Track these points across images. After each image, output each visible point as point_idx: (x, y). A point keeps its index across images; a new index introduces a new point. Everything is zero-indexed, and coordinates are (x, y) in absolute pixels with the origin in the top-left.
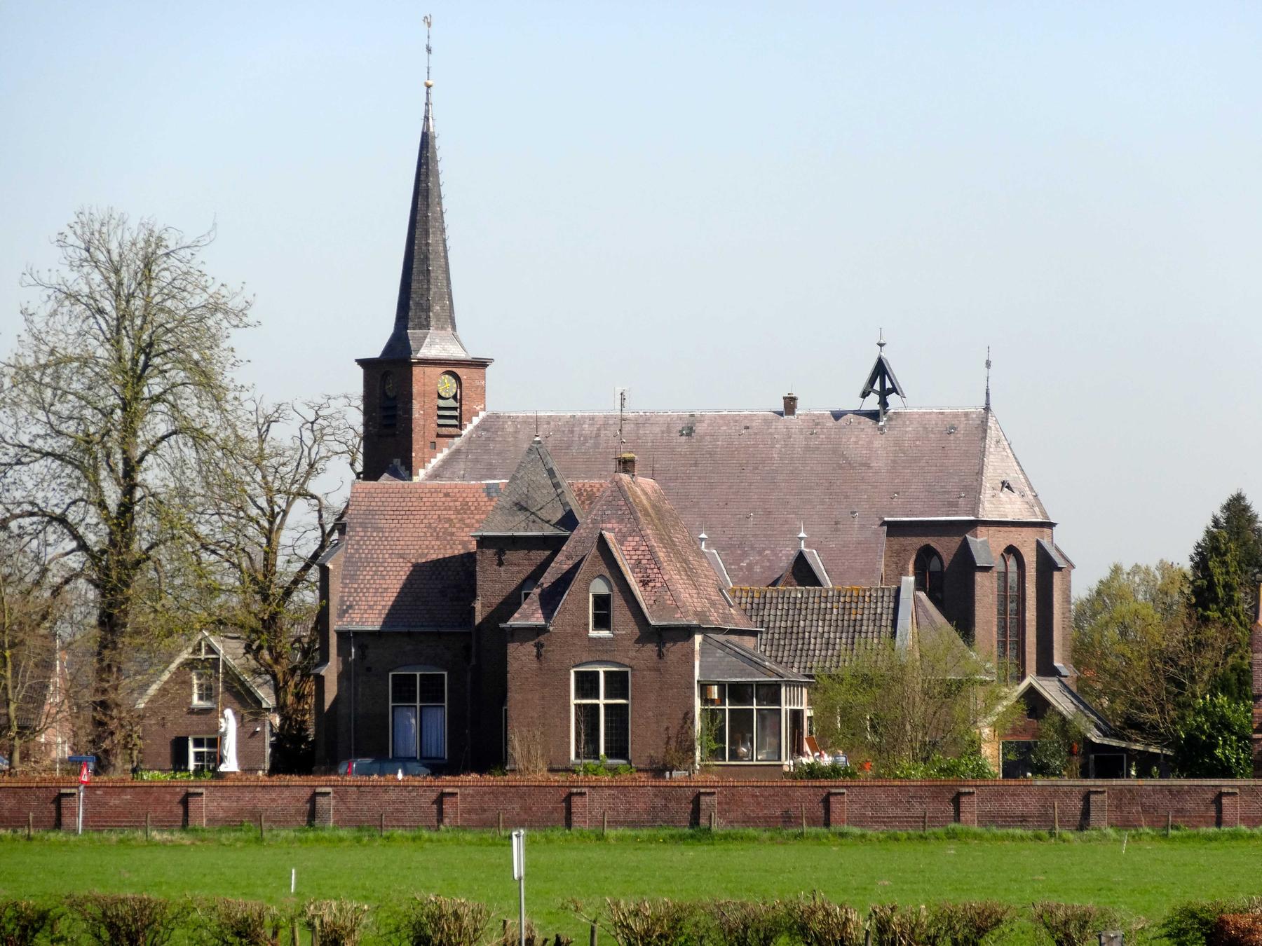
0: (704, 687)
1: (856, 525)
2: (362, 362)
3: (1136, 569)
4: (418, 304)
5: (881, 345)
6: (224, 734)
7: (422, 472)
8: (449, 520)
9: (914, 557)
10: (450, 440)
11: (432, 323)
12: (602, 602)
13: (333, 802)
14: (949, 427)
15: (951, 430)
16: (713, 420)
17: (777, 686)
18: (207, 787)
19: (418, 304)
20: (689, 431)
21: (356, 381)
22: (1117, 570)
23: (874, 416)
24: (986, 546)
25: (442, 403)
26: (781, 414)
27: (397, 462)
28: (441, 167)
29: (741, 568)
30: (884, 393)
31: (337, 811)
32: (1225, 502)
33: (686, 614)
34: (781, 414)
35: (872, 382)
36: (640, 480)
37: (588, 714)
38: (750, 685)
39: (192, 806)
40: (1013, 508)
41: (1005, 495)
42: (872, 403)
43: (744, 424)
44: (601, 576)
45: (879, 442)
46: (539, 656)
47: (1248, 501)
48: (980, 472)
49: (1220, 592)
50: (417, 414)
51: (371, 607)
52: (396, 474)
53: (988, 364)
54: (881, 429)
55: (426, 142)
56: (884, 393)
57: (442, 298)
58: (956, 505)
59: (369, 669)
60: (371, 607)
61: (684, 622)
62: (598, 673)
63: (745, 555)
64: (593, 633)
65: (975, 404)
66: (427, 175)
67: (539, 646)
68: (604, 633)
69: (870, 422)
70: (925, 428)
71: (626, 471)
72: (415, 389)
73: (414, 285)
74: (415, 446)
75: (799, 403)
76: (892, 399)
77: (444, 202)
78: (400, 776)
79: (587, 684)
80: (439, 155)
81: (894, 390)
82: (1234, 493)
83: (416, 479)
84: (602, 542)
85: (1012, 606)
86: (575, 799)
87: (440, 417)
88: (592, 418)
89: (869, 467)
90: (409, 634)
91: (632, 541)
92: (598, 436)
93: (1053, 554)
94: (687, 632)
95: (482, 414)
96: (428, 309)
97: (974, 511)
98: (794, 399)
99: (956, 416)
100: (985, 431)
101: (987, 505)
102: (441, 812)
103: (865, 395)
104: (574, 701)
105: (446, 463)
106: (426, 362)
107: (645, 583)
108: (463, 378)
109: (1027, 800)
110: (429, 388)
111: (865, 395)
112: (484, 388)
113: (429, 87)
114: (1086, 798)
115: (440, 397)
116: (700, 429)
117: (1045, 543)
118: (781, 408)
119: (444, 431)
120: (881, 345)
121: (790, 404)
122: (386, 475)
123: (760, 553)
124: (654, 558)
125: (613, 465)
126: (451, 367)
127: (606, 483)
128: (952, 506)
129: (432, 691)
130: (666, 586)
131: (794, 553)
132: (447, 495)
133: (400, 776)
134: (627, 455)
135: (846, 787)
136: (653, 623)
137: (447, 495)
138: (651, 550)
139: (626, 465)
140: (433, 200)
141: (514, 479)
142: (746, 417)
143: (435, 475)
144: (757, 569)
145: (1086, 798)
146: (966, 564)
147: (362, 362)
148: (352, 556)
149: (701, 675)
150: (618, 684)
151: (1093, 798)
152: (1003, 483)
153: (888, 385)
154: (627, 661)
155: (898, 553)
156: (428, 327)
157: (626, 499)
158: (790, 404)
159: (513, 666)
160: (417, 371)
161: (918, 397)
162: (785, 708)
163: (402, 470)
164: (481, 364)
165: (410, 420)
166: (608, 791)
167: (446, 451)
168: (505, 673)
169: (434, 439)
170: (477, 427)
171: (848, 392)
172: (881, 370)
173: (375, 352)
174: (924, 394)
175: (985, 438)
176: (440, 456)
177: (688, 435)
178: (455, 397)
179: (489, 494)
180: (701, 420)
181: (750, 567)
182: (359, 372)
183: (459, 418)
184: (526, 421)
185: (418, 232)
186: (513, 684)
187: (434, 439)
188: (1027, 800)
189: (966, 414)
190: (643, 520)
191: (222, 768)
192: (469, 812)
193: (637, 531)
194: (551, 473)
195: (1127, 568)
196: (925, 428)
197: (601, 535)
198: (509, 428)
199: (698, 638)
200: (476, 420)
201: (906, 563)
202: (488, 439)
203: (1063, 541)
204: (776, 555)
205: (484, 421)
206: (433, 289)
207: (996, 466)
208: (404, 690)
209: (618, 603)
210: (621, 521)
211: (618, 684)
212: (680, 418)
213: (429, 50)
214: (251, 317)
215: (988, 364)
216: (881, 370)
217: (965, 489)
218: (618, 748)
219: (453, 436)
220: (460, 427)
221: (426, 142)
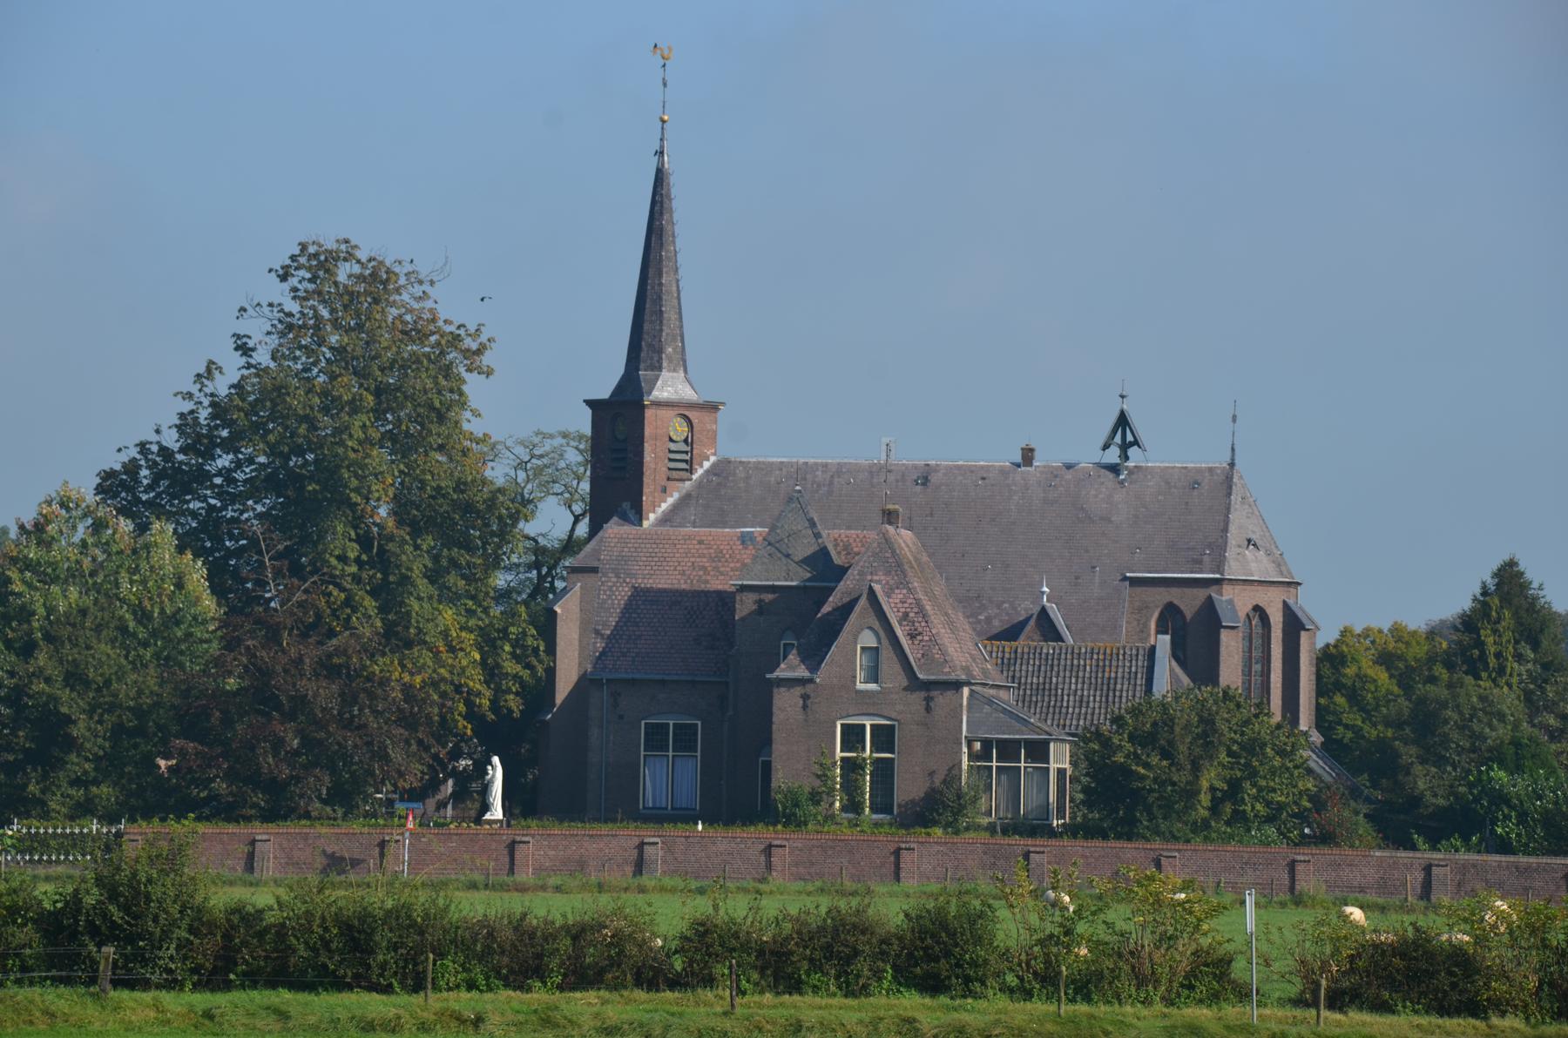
0: (970, 743)
1: (1097, 580)
2: (589, 403)
3: (1366, 633)
4: (650, 345)
5: (1122, 397)
6: (491, 781)
7: (652, 516)
8: (704, 568)
9: (1156, 615)
10: (680, 484)
11: (665, 364)
12: (874, 652)
13: (661, 853)
14: (1193, 481)
15: (1195, 485)
16: (949, 469)
17: (1046, 743)
18: (533, 836)
19: (650, 345)
20: (925, 481)
21: (583, 422)
22: (1345, 632)
23: (1114, 469)
24: (1236, 603)
25: (673, 446)
26: (1019, 466)
27: (626, 505)
28: (675, 204)
29: (979, 622)
30: (1125, 447)
31: (664, 862)
32: (1495, 568)
33: (953, 669)
34: (1019, 466)
35: (1114, 432)
36: (903, 532)
37: (851, 767)
38: (1018, 742)
39: (518, 855)
40: (1256, 565)
41: (1249, 553)
42: (1113, 456)
43: (982, 474)
44: (870, 628)
45: (1119, 496)
46: (805, 707)
47: (1522, 567)
48: (1225, 530)
49: (1492, 662)
50: (648, 457)
51: (624, 655)
52: (625, 518)
53: (1234, 419)
54: (1122, 482)
55: (660, 177)
56: (1125, 447)
57: (674, 340)
58: (1200, 562)
59: (621, 717)
60: (624, 655)
61: (953, 677)
62: (864, 726)
63: (983, 608)
64: (860, 686)
65: (1220, 460)
66: (661, 214)
67: (805, 697)
68: (873, 686)
69: (1111, 476)
70: (1168, 483)
71: (890, 523)
72: (648, 432)
73: (646, 327)
74: (646, 490)
75: (1036, 454)
76: (1133, 451)
77: (678, 241)
78: (700, 827)
79: (853, 736)
80: (674, 192)
81: (1136, 443)
82: (1507, 558)
83: (646, 524)
84: (871, 592)
85: (1257, 667)
86: (904, 853)
87: (673, 465)
88: (825, 465)
89: (1110, 521)
90: (663, 682)
91: (898, 595)
92: (831, 483)
93: (1300, 614)
94: (957, 686)
95: (713, 459)
96: (660, 351)
97: (1219, 569)
98: (1032, 450)
99: (1199, 471)
100: (1230, 488)
101: (1232, 563)
102: (769, 866)
103: (1106, 447)
104: (839, 754)
105: (675, 508)
106: (658, 404)
107: (912, 637)
108: (695, 421)
109: (1365, 870)
110: (661, 432)
111: (1106, 447)
112: (715, 432)
113: (664, 122)
114: (1428, 869)
115: (671, 440)
116: (934, 479)
117: (1291, 602)
118: (1018, 459)
119: (675, 474)
120: (1122, 397)
121: (1028, 455)
122: (615, 519)
123: (999, 607)
124: (922, 612)
125: (878, 518)
126: (683, 409)
127: (872, 535)
128: (1197, 564)
129: (685, 739)
130: (933, 640)
131: (1036, 610)
132: (700, 542)
133: (700, 827)
134: (890, 507)
135: (1179, 851)
136: (921, 676)
137: (700, 542)
138: (918, 602)
139: (890, 517)
140: (667, 238)
141: (773, 528)
142: (982, 467)
143: (665, 520)
144: (996, 623)
145: (1428, 869)
146: (1210, 620)
147: (589, 403)
148: (604, 601)
149: (968, 730)
150: (884, 738)
151: (1435, 870)
152: (1249, 541)
153: (1130, 438)
154: (894, 715)
155: (1140, 610)
156: (660, 369)
157: (894, 552)
158: (1028, 455)
159: (778, 717)
160: (649, 413)
161: (1161, 451)
162: (1053, 766)
163: (631, 515)
164: (713, 407)
165: (641, 463)
166: (937, 848)
167: (676, 495)
168: (771, 722)
169: (665, 482)
170: (707, 472)
171: (1086, 446)
172: (1123, 421)
173: (604, 392)
174: (1161, 451)
175: (1230, 494)
176: (670, 501)
177: (923, 484)
178: (686, 441)
179: (743, 543)
180: (936, 469)
181: (989, 620)
182: (588, 412)
183: (690, 462)
184: (758, 466)
185: (651, 272)
186: (778, 735)
187: (665, 482)
188: (1365, 870)
189: (1211, 470)
190: (910, 573)
191: (488, 816)
192: (797, 865)
193: (903, 583)
194: (813, 524)
195: (1358, 630)
196: (1168, 483)
197: (871, 588)
198: (741, 473)
199: (966, 691)
200: (707, 465)
201: (1148, 620)
202: (719, 484)
203: (1307, 603)
204: (1015, 609)
205: (714, 465)
206: (666, 330)
207: (1240, 523)
208: (656, 739)
209: (887, 654)
210: (888, 573)
211: (884, 738)
212: (915, 467)
213: (665, 85)
214: (487, 359)
215: (1234, 419)
216: (1123, 421)
217: (1210, 546)
218: (882, 804)
219: (682, 480)
220: (691, 471)
221: (660, 177)
